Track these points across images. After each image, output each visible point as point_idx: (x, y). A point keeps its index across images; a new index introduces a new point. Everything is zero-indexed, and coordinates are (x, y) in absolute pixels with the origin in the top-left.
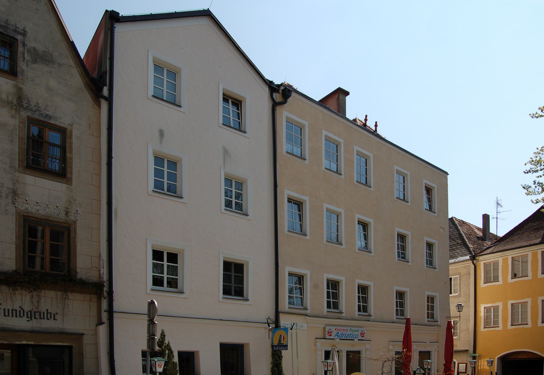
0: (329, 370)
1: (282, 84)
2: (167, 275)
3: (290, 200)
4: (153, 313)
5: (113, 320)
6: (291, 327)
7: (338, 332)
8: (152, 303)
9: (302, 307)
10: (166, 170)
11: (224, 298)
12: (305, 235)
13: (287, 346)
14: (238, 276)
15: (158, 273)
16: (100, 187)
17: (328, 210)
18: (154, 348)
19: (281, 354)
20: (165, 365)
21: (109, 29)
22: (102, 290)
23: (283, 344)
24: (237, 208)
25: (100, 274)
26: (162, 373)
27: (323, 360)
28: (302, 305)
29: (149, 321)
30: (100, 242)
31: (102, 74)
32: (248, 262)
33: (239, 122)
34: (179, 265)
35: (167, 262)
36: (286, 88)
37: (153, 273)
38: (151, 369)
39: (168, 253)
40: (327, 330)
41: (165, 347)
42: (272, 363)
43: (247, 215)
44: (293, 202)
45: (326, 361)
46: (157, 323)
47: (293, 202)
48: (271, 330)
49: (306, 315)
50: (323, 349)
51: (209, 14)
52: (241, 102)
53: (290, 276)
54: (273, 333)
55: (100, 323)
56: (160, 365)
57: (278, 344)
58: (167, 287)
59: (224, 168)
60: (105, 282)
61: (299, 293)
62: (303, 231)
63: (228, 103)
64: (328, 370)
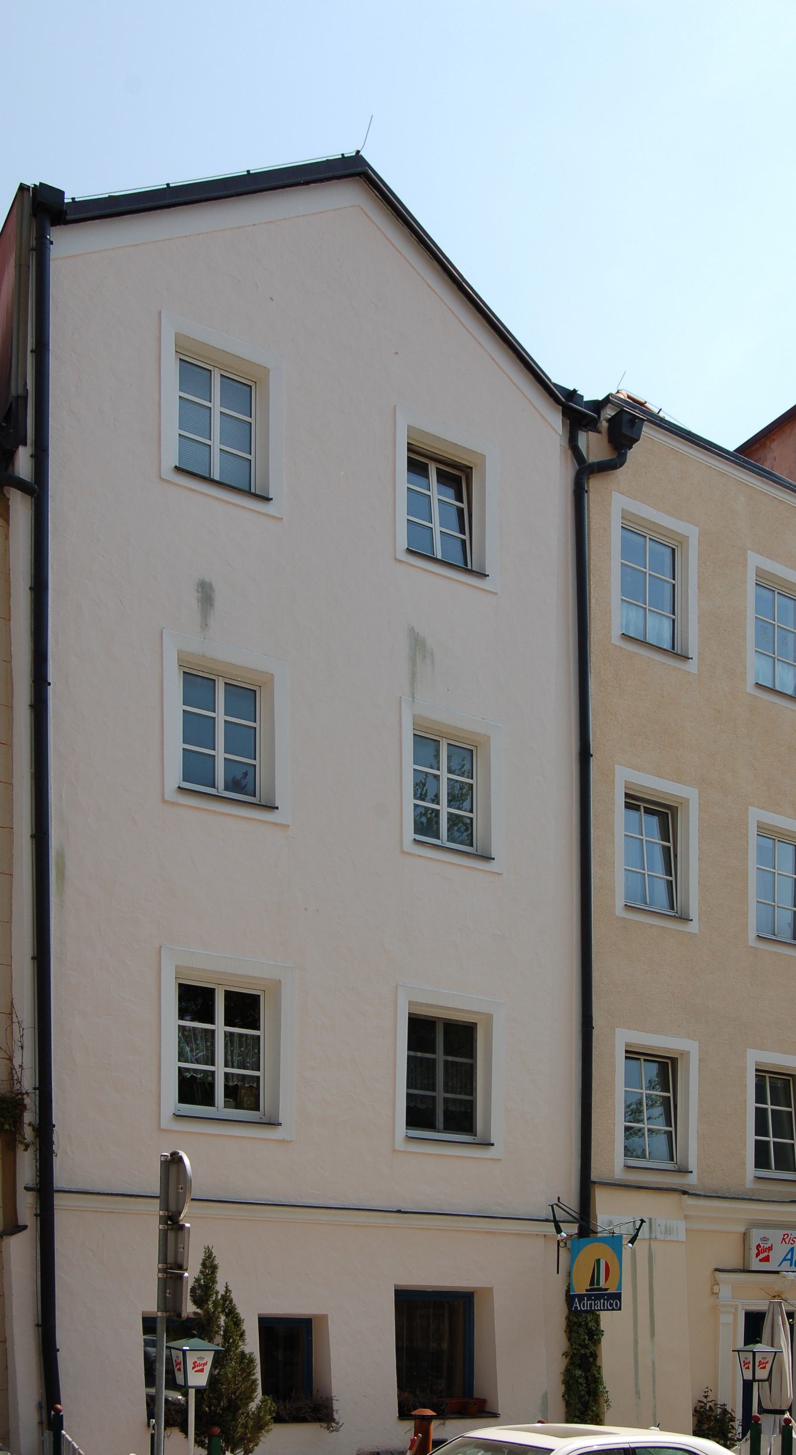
0: (757, 1378)
1: (607, 400)
2: (226, 1066)
3: (633, 802)
4: (178, 1193)
5: (53, 1215)
6: (633, 1233)
7: (792, 1250)
8: (175, 1160)
9: (669, 1166)
10: (220, 717)
11: (409, 1138)
12: (685, 918)
13: (618, 1296)
14: (457, 1063)
15: (198, 1061)
16: (11, 784)
17: (764, 831)
18: (181, 1311)
19: (598, 1323)
20: (217, 1363)
21: (32, 249)
22: (17, 1121)
23: (607, 1289)
24: (457, 834)
25: (12, 1068)
26: (205, 1390)
27: (740, 1344)
28: (672, 1159)
29: (164, 1220)
30: (11, 966)
31: (11, 404)
32: (489, 1018)
33: (463, 542)
34: (264, 1032)
35: (226, 1025)
36: (621, 412)
37: (179, 1061)
38: (170, 1372)
39: (229, 995)
40: (755, 1239)
41: (215, 1303)
42: (565, 1354)
43: (487, 858)
44: (644, 807)
45: (750, 1347)
46: (189, 1228)
47: (644, 807)
48: (566, 1244)
49: (685, 1193)
50: (740, 1307)
51: (359, 170)
52: (467, 471)
53: (630, 1062)
54: (574, 1254)
55: (15, 1228)
56: (200, 1365)
57: (587, 1290)
58: (225, 1107)
59: (413, 702)
60: (27, 1093)
61: (662, 1120)
62: (678, 904)
63: (426, 476)
64: (754, 1380)
